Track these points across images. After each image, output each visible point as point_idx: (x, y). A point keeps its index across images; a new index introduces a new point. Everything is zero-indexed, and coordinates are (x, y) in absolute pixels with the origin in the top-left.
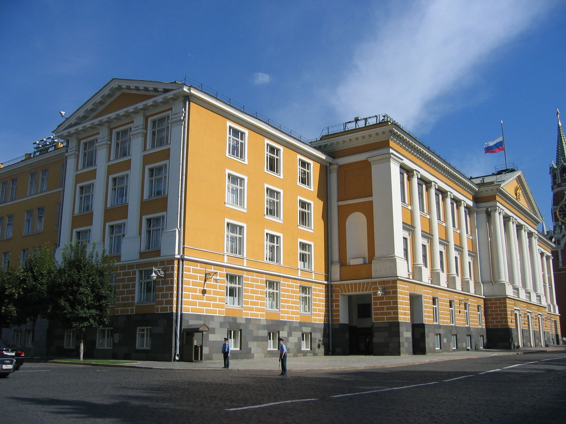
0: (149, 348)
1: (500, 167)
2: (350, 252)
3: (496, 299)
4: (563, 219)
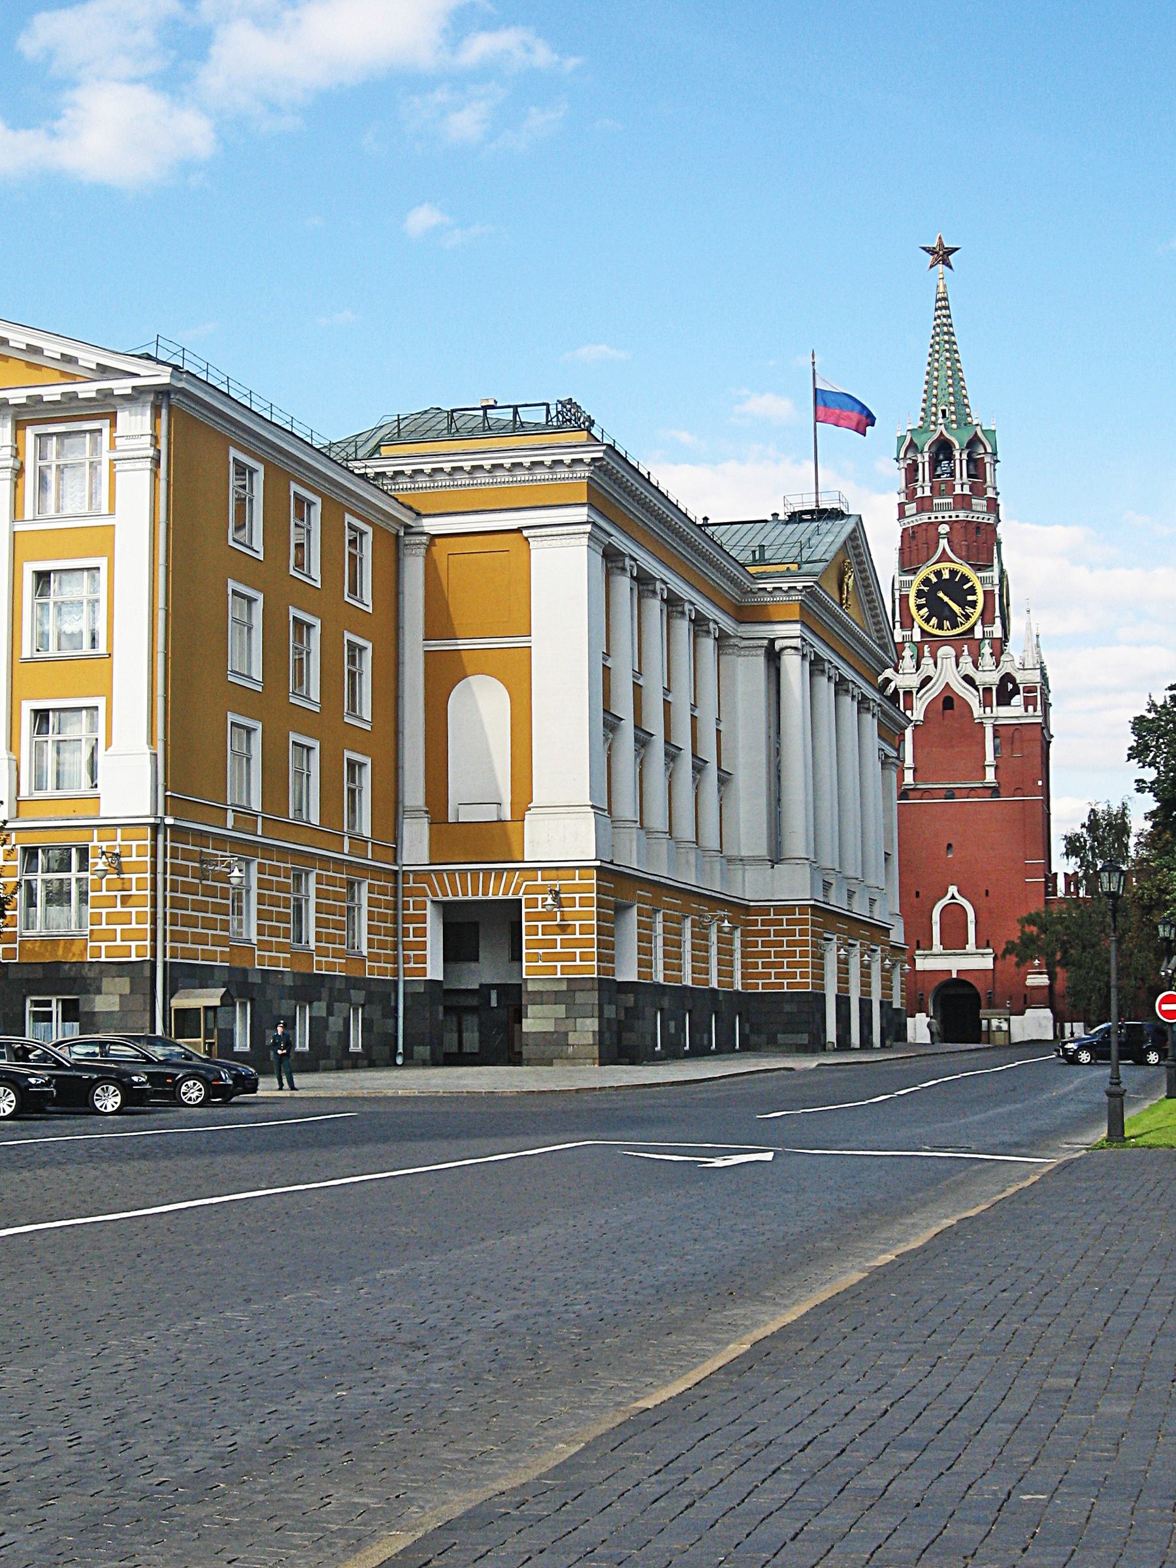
0: (247, 1048)
2: (458, 788)
3: (779, 910)
4: (927, 620)
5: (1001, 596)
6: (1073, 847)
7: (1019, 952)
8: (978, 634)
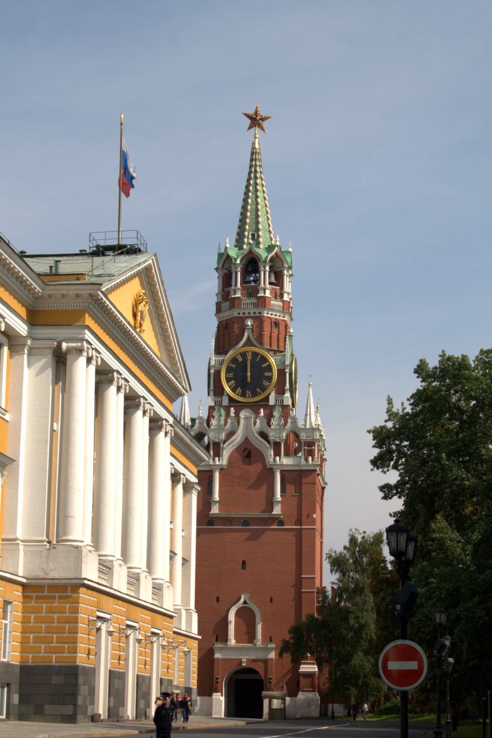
1: (102, 236)
5: (291, 374)
6: (337, 563)
7: (295, 647)
8: (272, 402)
